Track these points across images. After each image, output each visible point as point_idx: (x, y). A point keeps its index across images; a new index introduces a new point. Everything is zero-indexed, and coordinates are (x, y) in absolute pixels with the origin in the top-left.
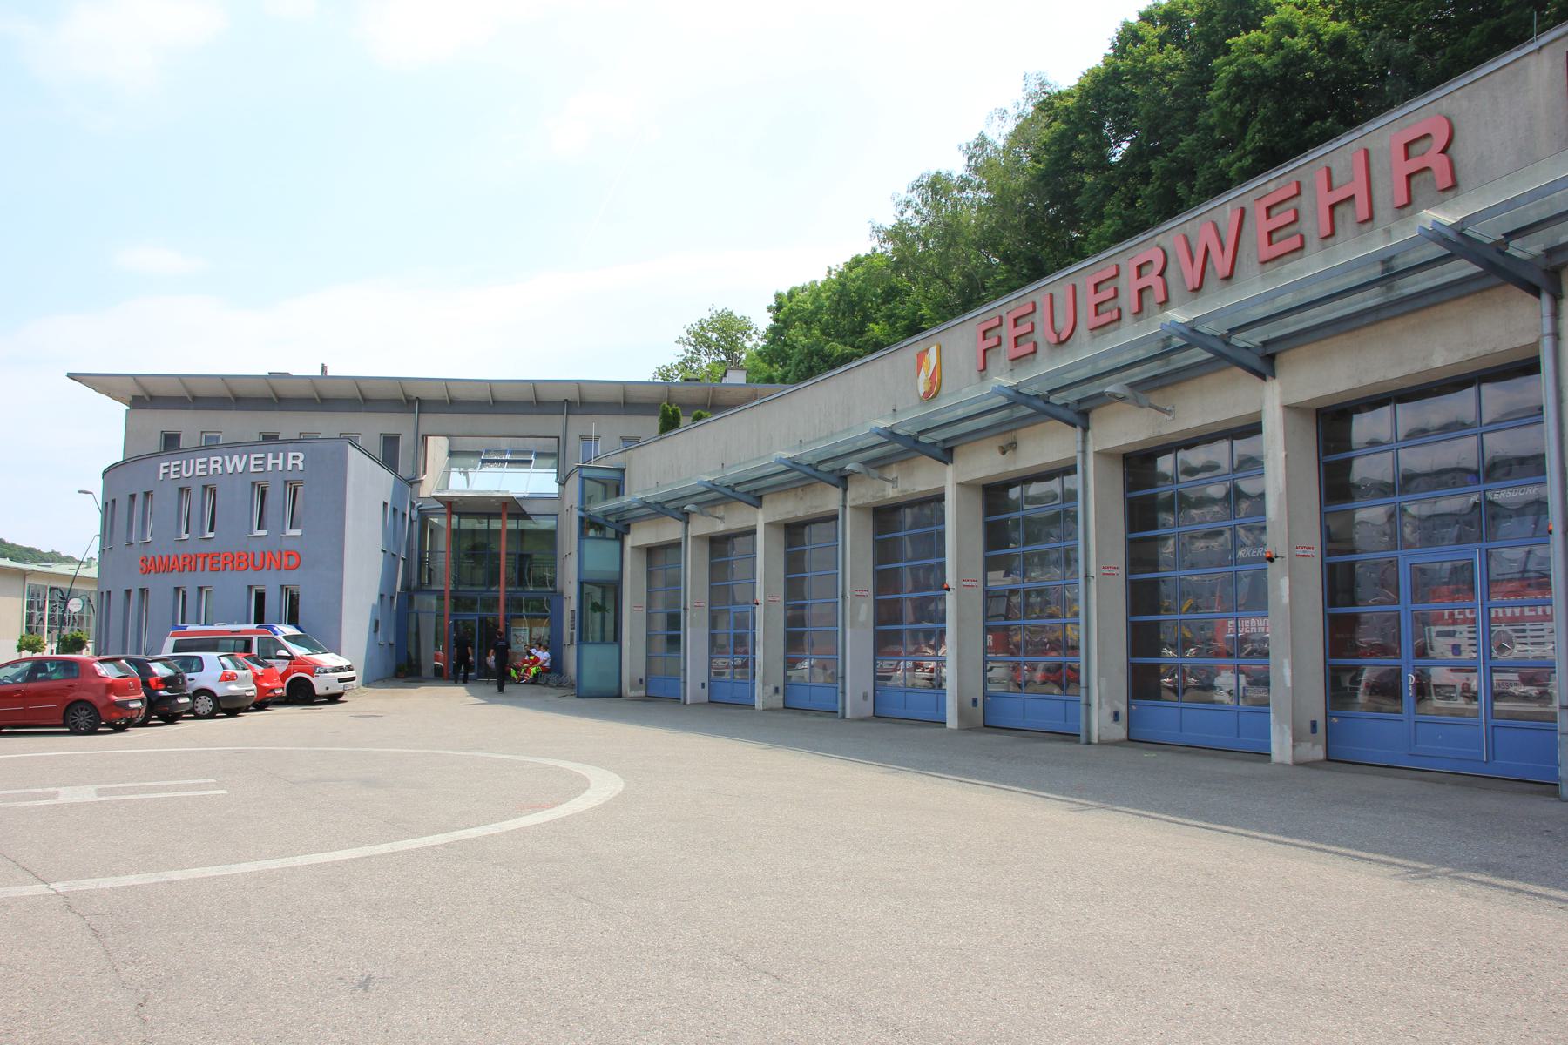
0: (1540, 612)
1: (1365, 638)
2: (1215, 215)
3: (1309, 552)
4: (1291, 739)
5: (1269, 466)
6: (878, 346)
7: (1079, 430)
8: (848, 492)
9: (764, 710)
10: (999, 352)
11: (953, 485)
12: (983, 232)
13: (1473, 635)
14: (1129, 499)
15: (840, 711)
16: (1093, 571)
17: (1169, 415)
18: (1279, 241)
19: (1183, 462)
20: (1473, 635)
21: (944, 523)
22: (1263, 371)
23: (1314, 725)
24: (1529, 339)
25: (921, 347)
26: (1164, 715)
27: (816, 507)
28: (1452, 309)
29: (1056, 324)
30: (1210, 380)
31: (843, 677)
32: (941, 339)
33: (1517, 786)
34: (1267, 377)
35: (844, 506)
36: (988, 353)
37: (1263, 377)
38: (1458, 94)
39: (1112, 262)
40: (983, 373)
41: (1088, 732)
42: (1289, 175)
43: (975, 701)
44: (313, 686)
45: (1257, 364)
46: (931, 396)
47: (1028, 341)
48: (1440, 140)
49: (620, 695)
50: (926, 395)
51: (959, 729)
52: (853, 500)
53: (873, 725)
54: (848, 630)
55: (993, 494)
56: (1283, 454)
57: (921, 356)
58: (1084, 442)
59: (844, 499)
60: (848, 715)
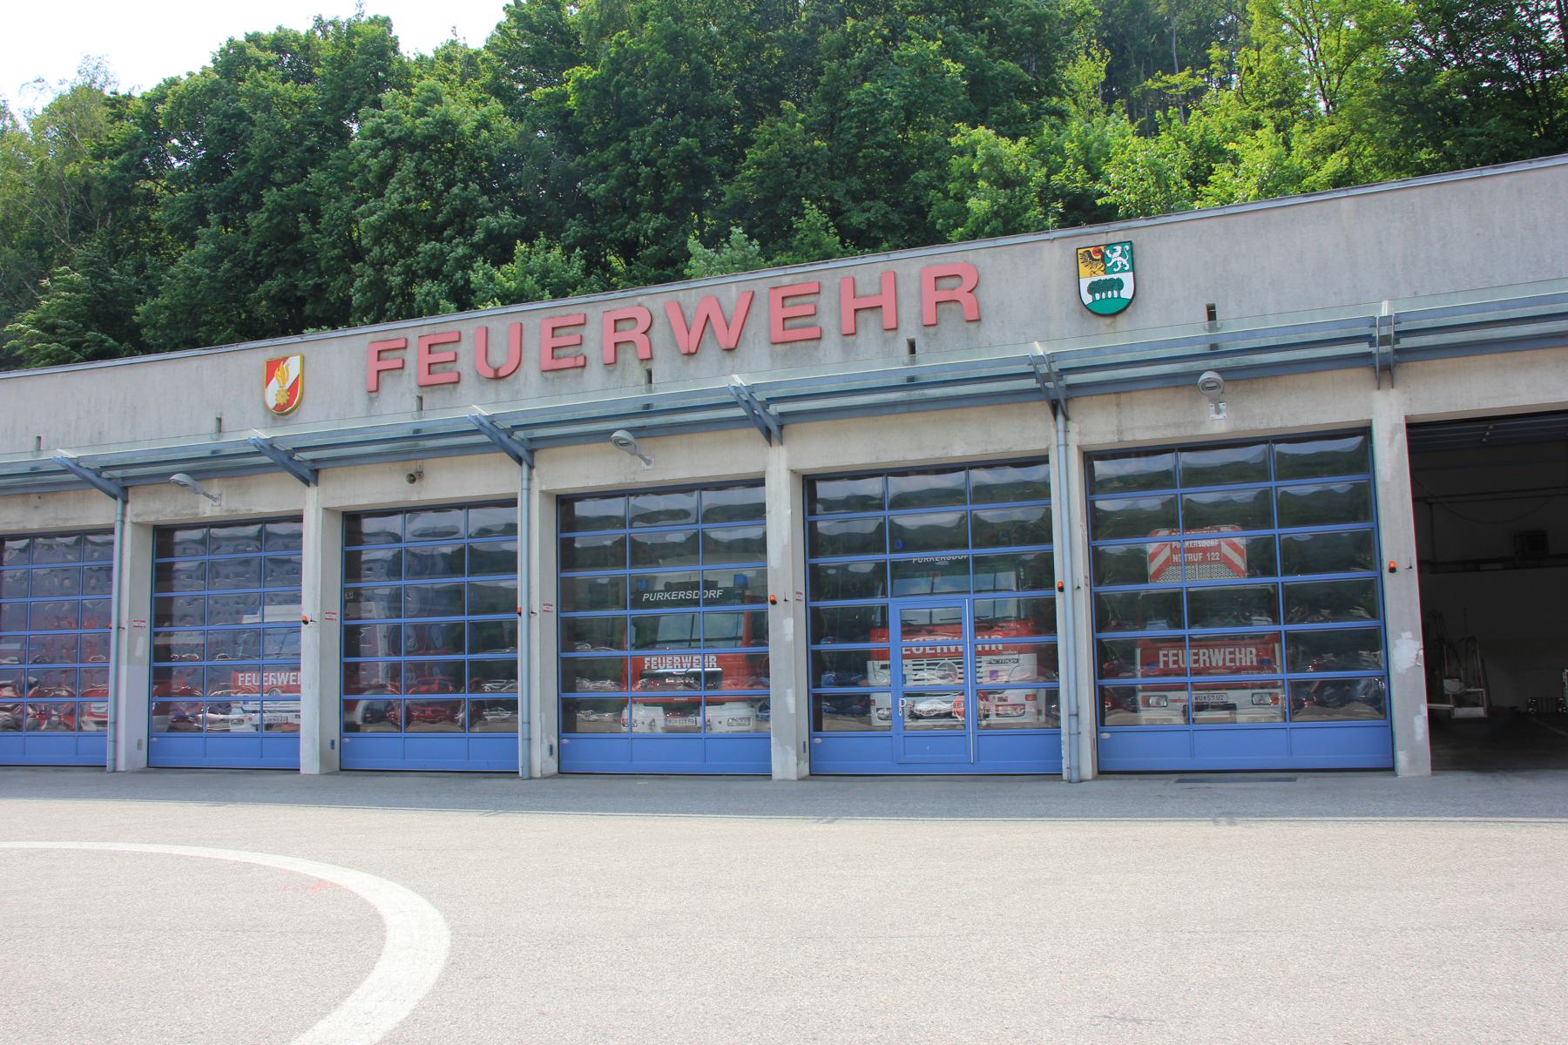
0: (939, 651)
1: (177, 686)
2: (719, 291)
3: (142, 624)
4: (795, 758)
5: (771, 518)
6: (1421, 171)
7: (119, 502)
8: (129, 507)
9: (799, 780)
10: (401, 375)
11: (317, 510)
12: (500, 233)
13: (978, 665)
14: (561, 539)
15: (109, 764)
16: (125, 624)
17: (648, 464)
18: (791, 328)
19: (634, 506)
20: (978, 665)
21: (301, 548)
22: (308, 478)
23: (333, 742)
24: (112, 521)
25: (272, 354)
26: (182, 745)
27: (66, 520)
28: (973, 413)
29: (490, 359)
30: (275, 476)
31: (115, 723)
32: (304, 348)
33: (464, 775)
34: (311, 484)
35: (123, 522)
36: (381, 375)
37: (307, 482)
38: (983, 251)
39: (582, 309)
40: (374, 395)
41: (530, 767)
42: (809, 274)
43: (333, 742)
44: (367, 968)
45: (306, 472)
46: (282, 411)
47: (450, 371)
48: (643, 324)
49: (1057, 775)
50: (279, 408)
51: (321, 774)
52: (137, 515)
53: (149, 772)
54: (124, 669)
55: (163, 537)
56: (789, 512)
57: (272, 367)
58: (124, 509)
59: (124, 514)
60: (122, 766)
